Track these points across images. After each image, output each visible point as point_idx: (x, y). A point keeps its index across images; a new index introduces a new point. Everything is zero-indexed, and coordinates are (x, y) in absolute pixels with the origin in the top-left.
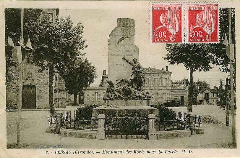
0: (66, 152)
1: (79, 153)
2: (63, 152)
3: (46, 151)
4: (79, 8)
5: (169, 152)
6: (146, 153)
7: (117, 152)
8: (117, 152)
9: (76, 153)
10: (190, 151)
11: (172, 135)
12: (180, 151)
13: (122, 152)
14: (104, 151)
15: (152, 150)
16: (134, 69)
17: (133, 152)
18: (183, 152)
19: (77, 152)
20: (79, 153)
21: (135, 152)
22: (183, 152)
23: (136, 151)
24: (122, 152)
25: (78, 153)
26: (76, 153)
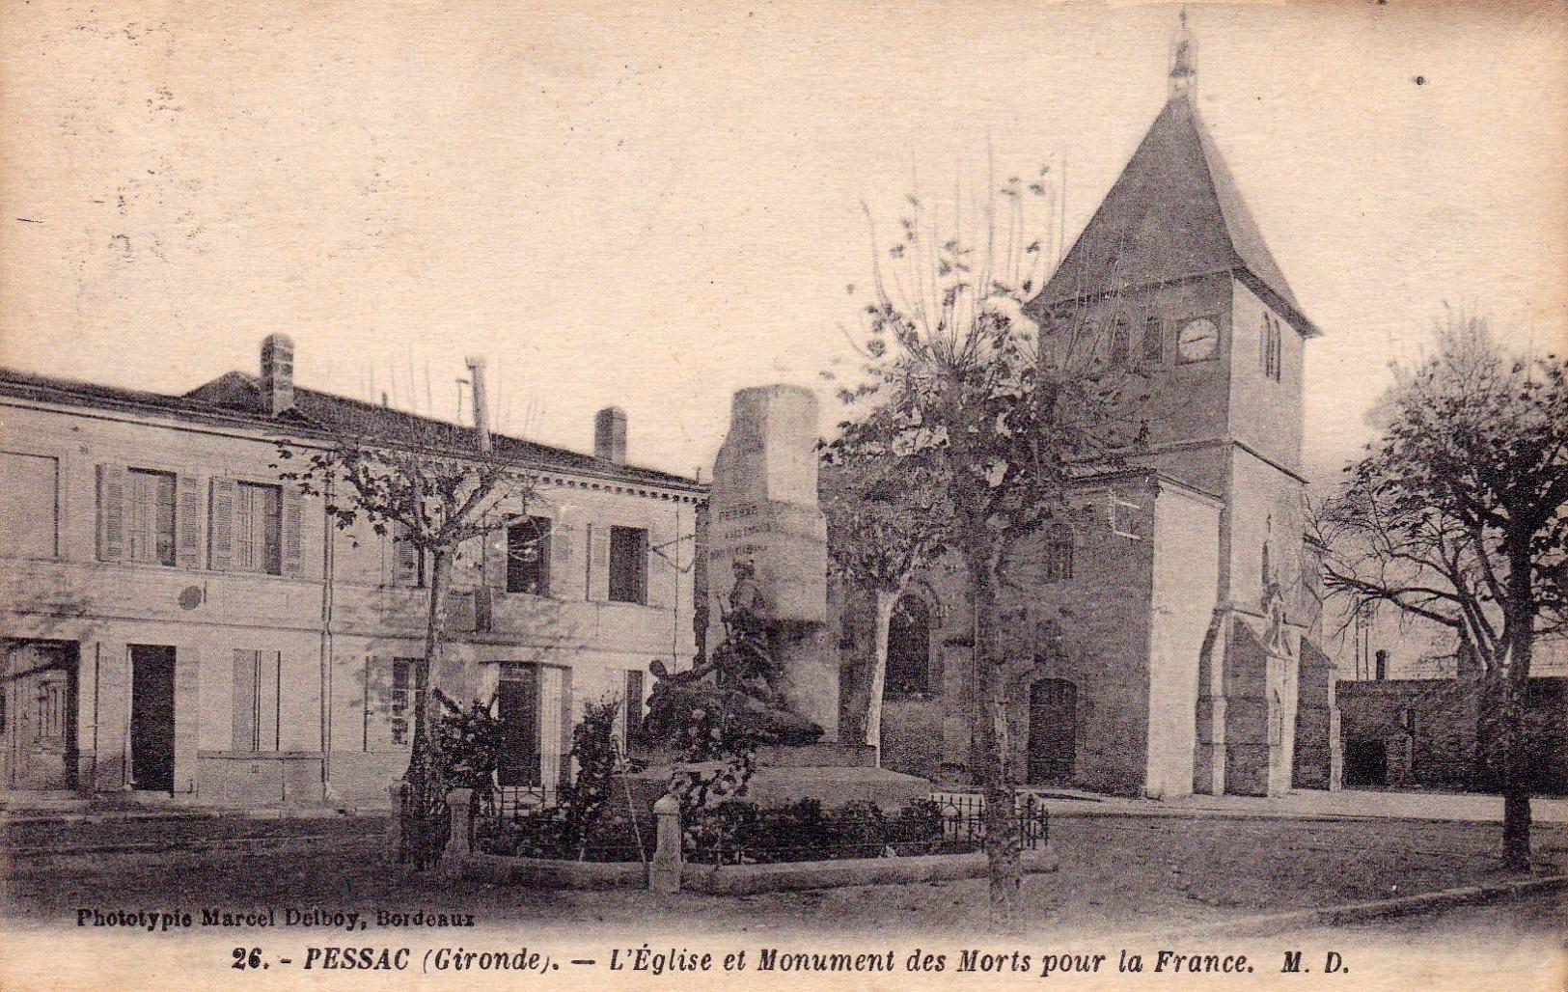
0: (376, 957)
1: (463, 962)
2: (357, 958)
3: (884, 376)
4: (791, 803)
5: (988, 963)
6: (1037, 965)
7: (853, 961)
8: (853, 961)
9: (441, 964)
10: (1335, 960)
11: (786, 886)
12: (1267, 957)
13: (884, 963)
14: (966, 953)
15: (1078, 946)
16: (158, 709)
17: (954, 960)
18: (1292, 962)
19: (444, 956)
20: (463, 962)
21: (767, 960)
22: (1292, 962)
23: (975, 953)
24: (884, 963)
25: (452, 963)
26: (441, 964)
